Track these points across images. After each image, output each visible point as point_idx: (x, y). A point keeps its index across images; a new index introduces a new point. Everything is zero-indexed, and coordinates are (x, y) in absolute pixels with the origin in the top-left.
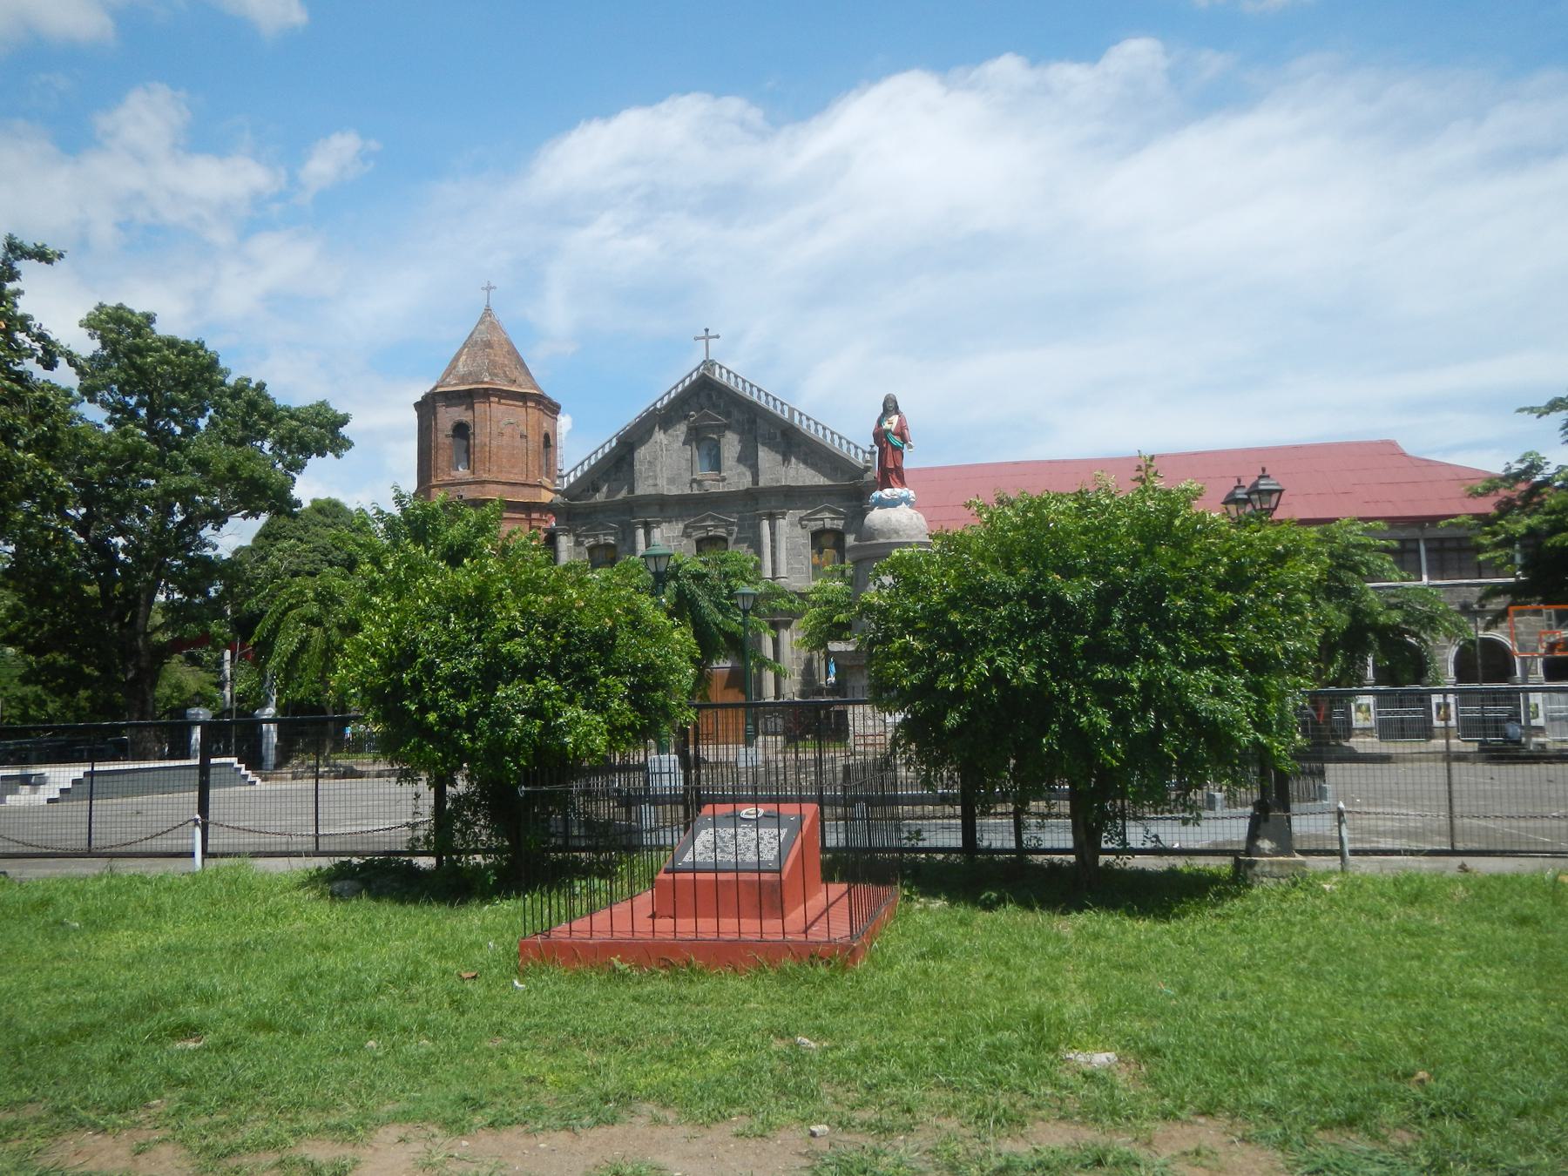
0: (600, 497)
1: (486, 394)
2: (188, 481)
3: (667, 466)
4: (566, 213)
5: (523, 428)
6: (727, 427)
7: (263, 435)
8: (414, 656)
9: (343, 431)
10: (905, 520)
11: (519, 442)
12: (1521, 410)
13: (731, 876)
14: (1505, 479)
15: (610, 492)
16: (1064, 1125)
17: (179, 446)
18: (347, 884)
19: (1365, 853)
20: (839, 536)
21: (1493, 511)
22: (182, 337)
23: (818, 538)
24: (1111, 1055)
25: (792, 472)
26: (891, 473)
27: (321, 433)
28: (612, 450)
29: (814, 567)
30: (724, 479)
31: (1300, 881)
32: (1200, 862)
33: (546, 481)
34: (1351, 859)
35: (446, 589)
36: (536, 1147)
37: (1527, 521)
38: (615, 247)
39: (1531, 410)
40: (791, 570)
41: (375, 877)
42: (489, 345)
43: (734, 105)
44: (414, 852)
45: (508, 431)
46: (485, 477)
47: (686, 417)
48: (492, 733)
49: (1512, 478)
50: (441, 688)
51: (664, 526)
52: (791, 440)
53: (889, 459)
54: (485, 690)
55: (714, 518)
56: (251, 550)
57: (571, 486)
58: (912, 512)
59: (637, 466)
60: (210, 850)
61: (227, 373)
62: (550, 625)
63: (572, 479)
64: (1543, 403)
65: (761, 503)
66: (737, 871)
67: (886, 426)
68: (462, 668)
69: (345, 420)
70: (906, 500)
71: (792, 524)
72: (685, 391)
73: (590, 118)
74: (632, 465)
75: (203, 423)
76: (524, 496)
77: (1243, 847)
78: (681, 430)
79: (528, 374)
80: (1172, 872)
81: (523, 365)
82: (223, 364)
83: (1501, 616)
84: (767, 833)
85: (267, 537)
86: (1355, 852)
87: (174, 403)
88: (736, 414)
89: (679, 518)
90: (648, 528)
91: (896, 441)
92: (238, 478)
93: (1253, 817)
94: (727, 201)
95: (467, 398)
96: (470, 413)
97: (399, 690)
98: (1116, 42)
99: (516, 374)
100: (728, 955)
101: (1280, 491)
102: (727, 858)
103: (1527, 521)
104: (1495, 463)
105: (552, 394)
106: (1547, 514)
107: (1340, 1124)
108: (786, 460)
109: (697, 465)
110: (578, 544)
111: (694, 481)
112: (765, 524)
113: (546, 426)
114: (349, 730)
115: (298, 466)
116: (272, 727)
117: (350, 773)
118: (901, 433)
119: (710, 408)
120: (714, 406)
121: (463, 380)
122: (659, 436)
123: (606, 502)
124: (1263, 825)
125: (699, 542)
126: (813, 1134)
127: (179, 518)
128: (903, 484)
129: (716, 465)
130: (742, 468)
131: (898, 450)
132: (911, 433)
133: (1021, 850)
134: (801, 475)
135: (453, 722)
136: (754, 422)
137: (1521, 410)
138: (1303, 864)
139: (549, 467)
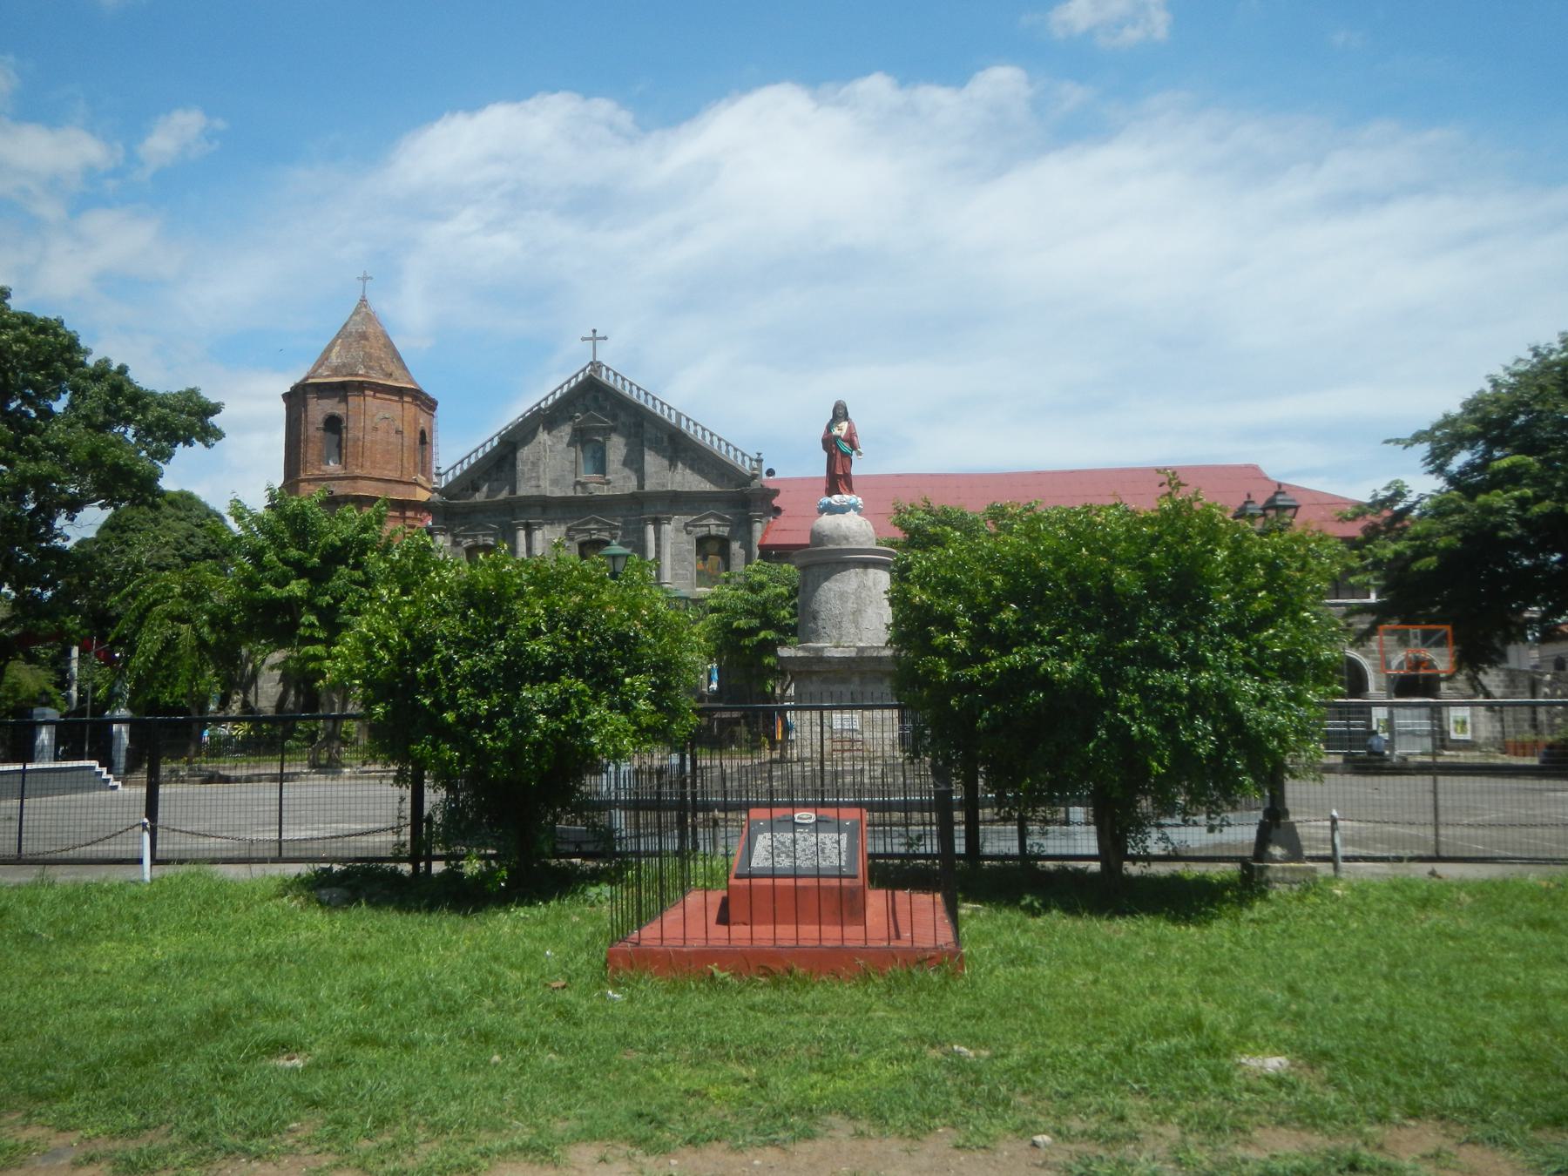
0: (480, 497)
1: (361, 387)
2: (45, 468)
3: (550, 467)
4: (427, 206)
5: (398, 424)
6: (614, 429)
7: (128, 421)
8: (430, 652)
9: (214, 420)
10: (854, 527)
11: (394, 438)
12: (1387, 442)
13: (813, 882)
14: (1371, 505)
15: (491, 492)
16: (1283, 1130)
17: (33, 429)
18: (336, 892)
19: (1356, 859)
20: (723, 545)
21: (1359, 535)
22: (39, 314)
23: (704, 545)
24: (1283, 1059)
25: (678, 478)
26: (838, 479)
27: (192, 420)
28: (493, 449)
29: (699, 573)
30: (608, 483)
31: (1310, 885)
32: (1081, 865)
33: (421, 479)
34: (1342, 864)
35: (459, 584)
36: (749, 1164)
37: (1394, 547)
38: (478, 243)
39: (1397, 441)
40: (675, 576)
41: (353, 883)
42: (364, 336)
43: (603, 107)
44: (397, 859)
45: (383, 425)
46: (358, 472)
47: (572, 418)
48: (516, 734)
49: (1379, 504)
50: (459, 686)
51: (546, 528)
52: (678, 444)
53: (838, 465)
54: (506, 690)
55: (597, 522)
56: (95, 541)
57: (449, 486)
58: (861, 519)
59: (520, 467)
60: (158, 856)
61: (87, 352)
62: (575, 622)
63: (450, 478)
64: (1408, 435)
65: (645, 508)
66: (818, 876)
67: (836, 432)
68: (484, 666)
69: (216, 409)
70: (854, 507)
71: (677, 530)
72: (571, 392)
73: (454, 110)
74: (514, 465)
75: (59, 406)
76: (399, 493)
77: (1249, 853)
78: (566, 431)
79: (405, 368)
80: (1175, 879)
81: (399, 359)
82: (83, 343)
83: (1362, 639)
84: (828, 838)
85: (113, 530)
86: (1347, 859)
87: (29, 384)
88: (623, 417)
89: (561, 520)
90: (529, 530)
91: (845, 447)
92: (101, 465)
93: (1262, 825)
94: (593, 203)
95: (341, 390)
96: (343, 406)
97: (412, 683)
98: (982, 68)
99: (391, 368)
100: (831, 963)
101: (1296, 507)
102: (784, 862)
103: (1394, 547)
104: (1362, 492)
105: (430, 390)
106: (1411, 539)
107: (1547, 1122)
108: (672, 465)
109: (582, 468)
110: (456, 544)
111: (578, 483)
112: (650, 529)
113: (423, 421)
114: (206, 733)
115: (166, 456)
116: (124, 728)
117: (212, 779)
118: (851, 440)
119: (597, 409)
120: (601, 409)
121: (336, 371)
122: (543, 436)
123: (487, 497)
124: (1274, 832)
125: (582, 545)
126: (1034, 1145)
127: (32, 506)
128: (851, 491)
129: (601, 468)
130: (627, 472)
131: (847, 456)
132: (860, 441)
133: (1025, 857)
134: (686, 480)
135: (471, 721)
136: (641, 426)
137: (1387, 442)
138: (1314, 870)
139: (424, 466)
